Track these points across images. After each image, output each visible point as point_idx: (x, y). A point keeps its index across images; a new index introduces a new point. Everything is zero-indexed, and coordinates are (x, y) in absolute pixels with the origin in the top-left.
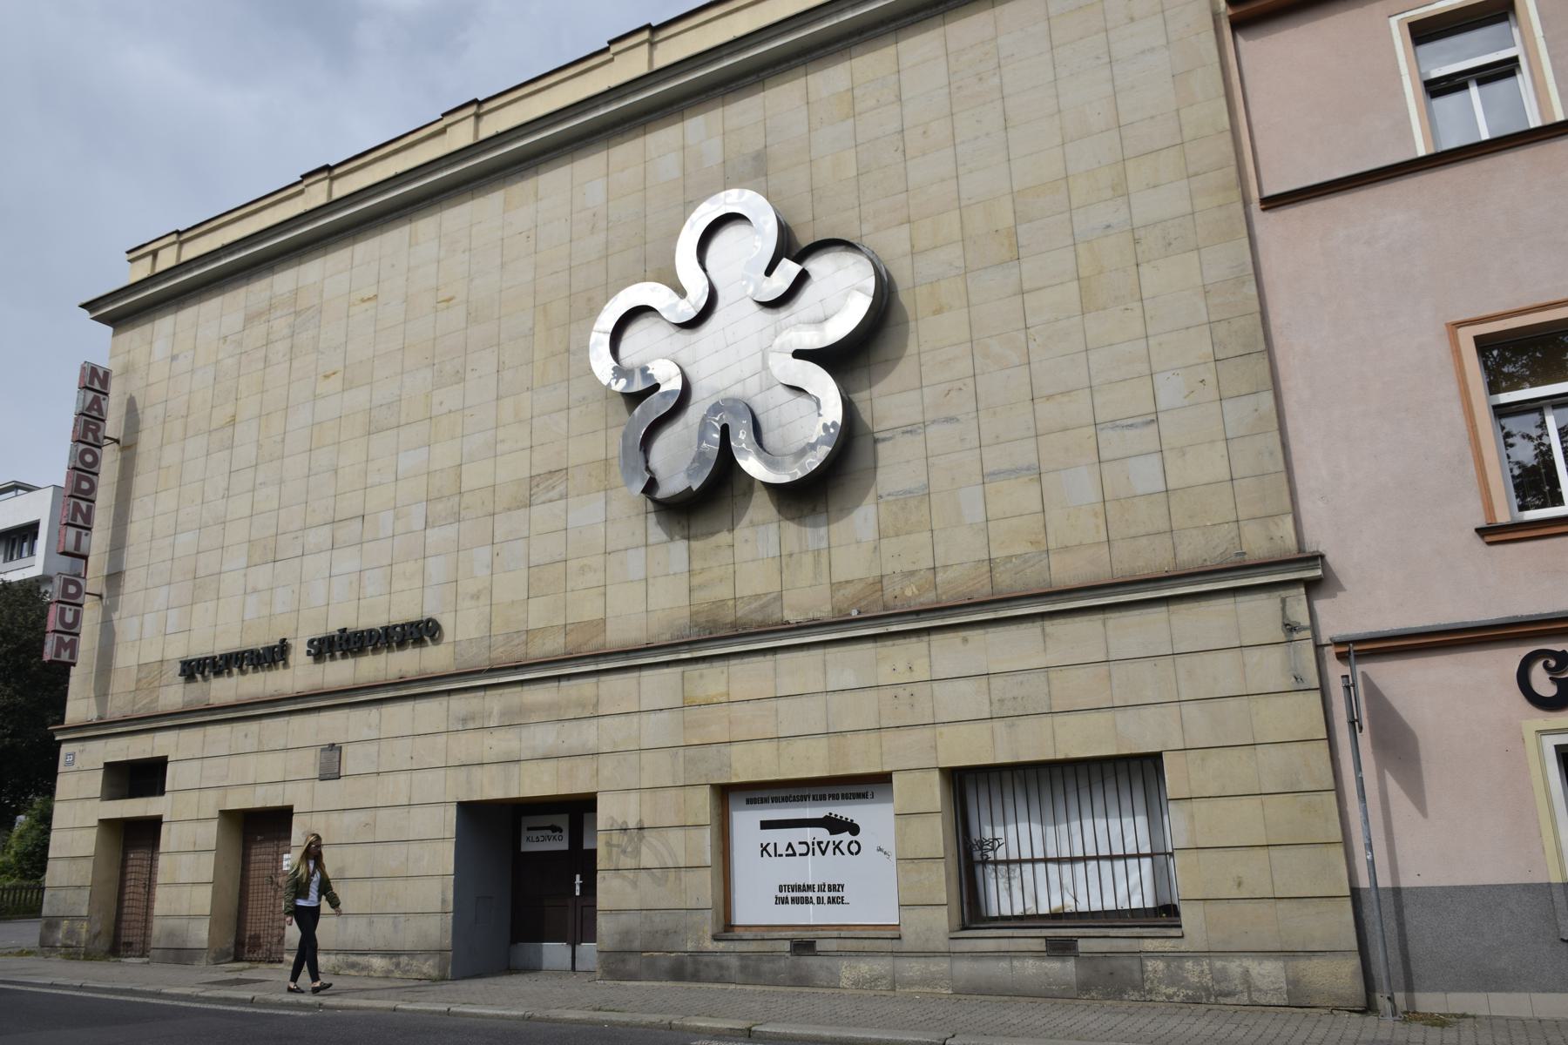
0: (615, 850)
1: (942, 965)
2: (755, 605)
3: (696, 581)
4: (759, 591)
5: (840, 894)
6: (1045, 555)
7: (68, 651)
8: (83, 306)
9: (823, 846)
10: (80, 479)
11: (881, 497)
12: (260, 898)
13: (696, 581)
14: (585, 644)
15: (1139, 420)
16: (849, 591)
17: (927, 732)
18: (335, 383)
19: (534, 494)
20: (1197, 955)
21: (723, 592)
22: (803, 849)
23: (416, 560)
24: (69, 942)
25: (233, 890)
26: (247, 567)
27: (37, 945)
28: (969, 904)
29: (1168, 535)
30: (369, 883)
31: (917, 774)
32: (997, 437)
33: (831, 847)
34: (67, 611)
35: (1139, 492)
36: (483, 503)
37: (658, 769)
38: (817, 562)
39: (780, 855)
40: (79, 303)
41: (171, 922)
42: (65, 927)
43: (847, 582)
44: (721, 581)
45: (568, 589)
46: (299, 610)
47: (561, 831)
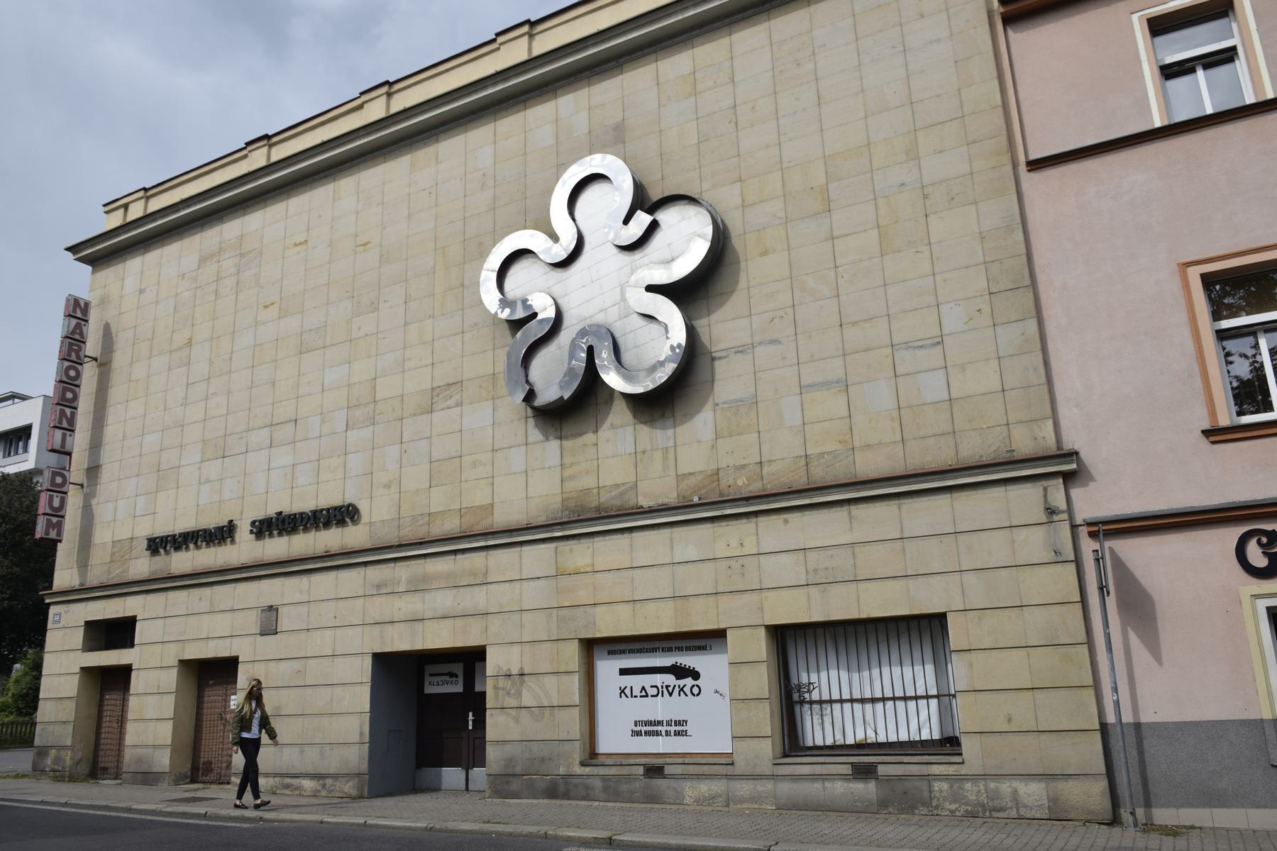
5: (684, 728)
7: (56, 530)
8: (68, 249)
10: (65, 390)
24: (56, 767)
26: (201, 462)
27: (30, 769)
28: (789, 736)
32: (812, 356)
34: (55, 498)
40: (65, 247)
41: (140, 751)
42: (53, 755)
46: (243, 497)
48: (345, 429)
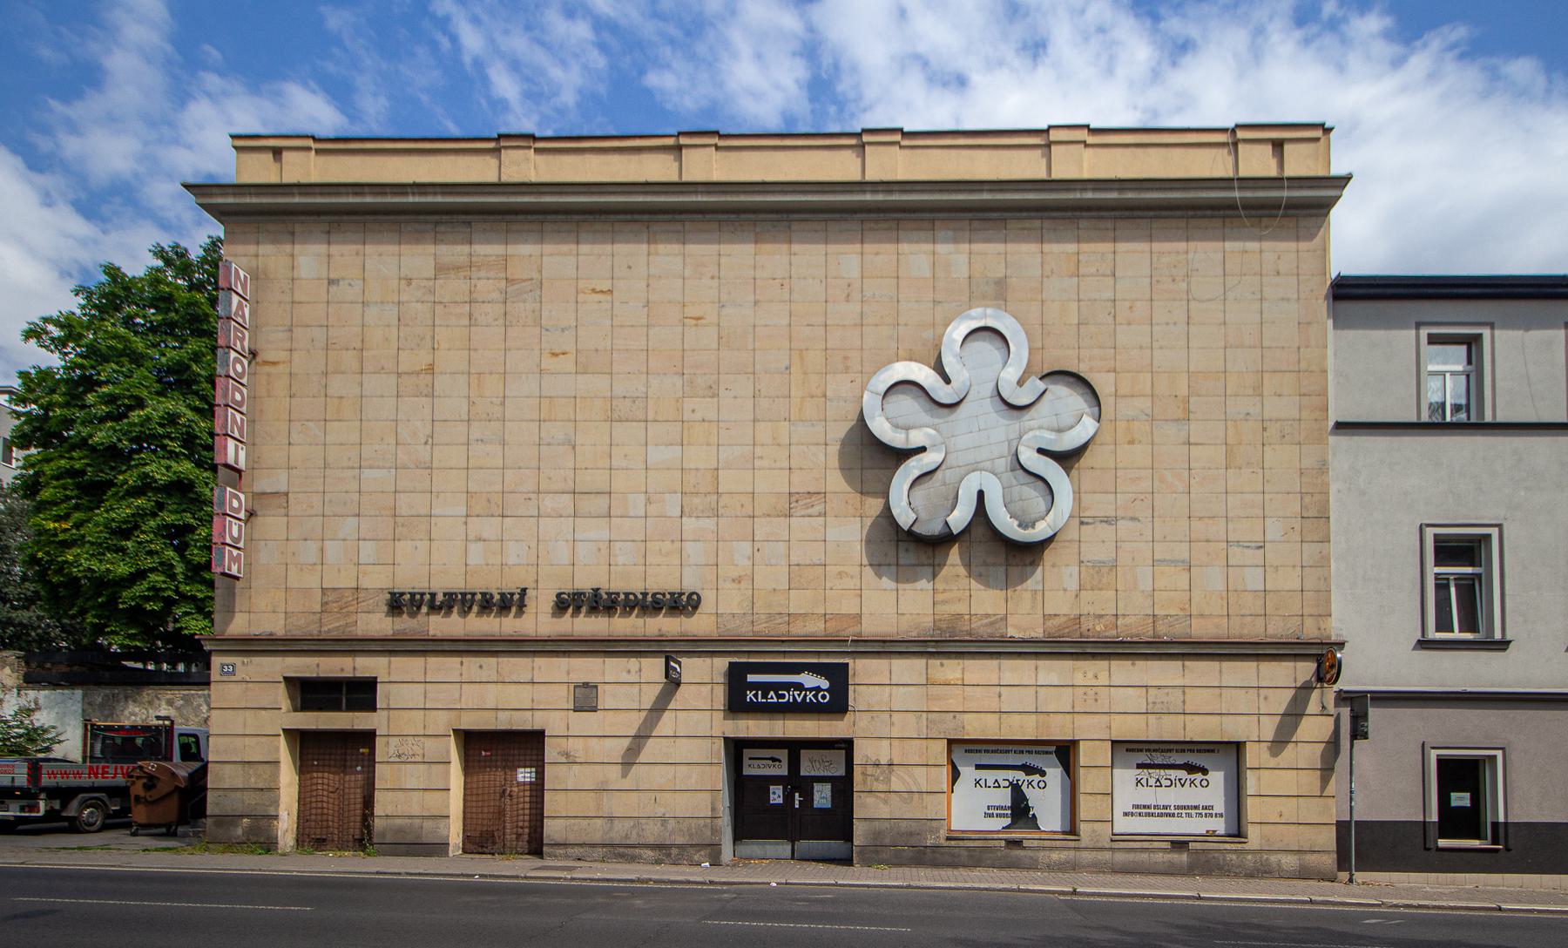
0: (869, 778)
1: (1107, 855)
2: (985, 621)
3: (939, 597)
4: (990, 612)
6: (1189, 618)
7: (237, 565)
9: (1182, 782)
11: (1083, 562)
12: (319, 811)
13: (939, 597)
14: (844, 630)
15: (1253, 544)
16: (1056, 622)
17: (1106, 717)
18: (567, 364)
19: (793, 508)
20: (1254, 852)
21: (962, 608)
22: (1169, 783)
23: (673, 541)
25: (1242, 780)
29: (1263, 617)
30: (635, 794)
31: (1097, 742)
33: (1188, 782)
34: (234, 525)
35: (1249, 589)
36: (742, 506)
37: (908, 725)
38: (1034, 599)
39: (989, 787)
41: (399, 821)
43: (1055, 615)
44: (959, 600)
45: (828, 587)
47: (780, 761)
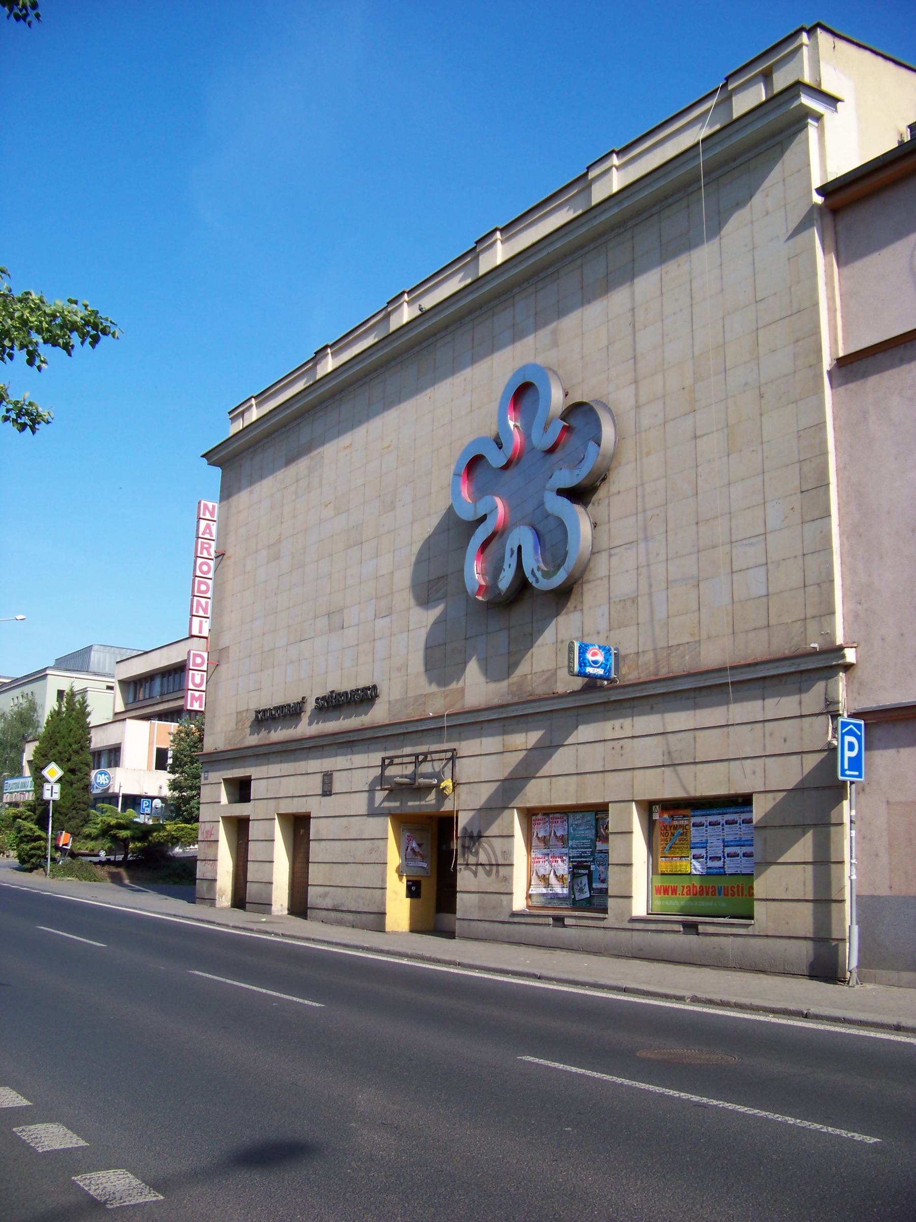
7: (198, 702)
8: (203, 456)
10: (200, 583)
26: (274, 649)
32: (677, 552)
34: (196, 676)
40: (201, 454)
46: (312, 677)
48: (373, 618)
